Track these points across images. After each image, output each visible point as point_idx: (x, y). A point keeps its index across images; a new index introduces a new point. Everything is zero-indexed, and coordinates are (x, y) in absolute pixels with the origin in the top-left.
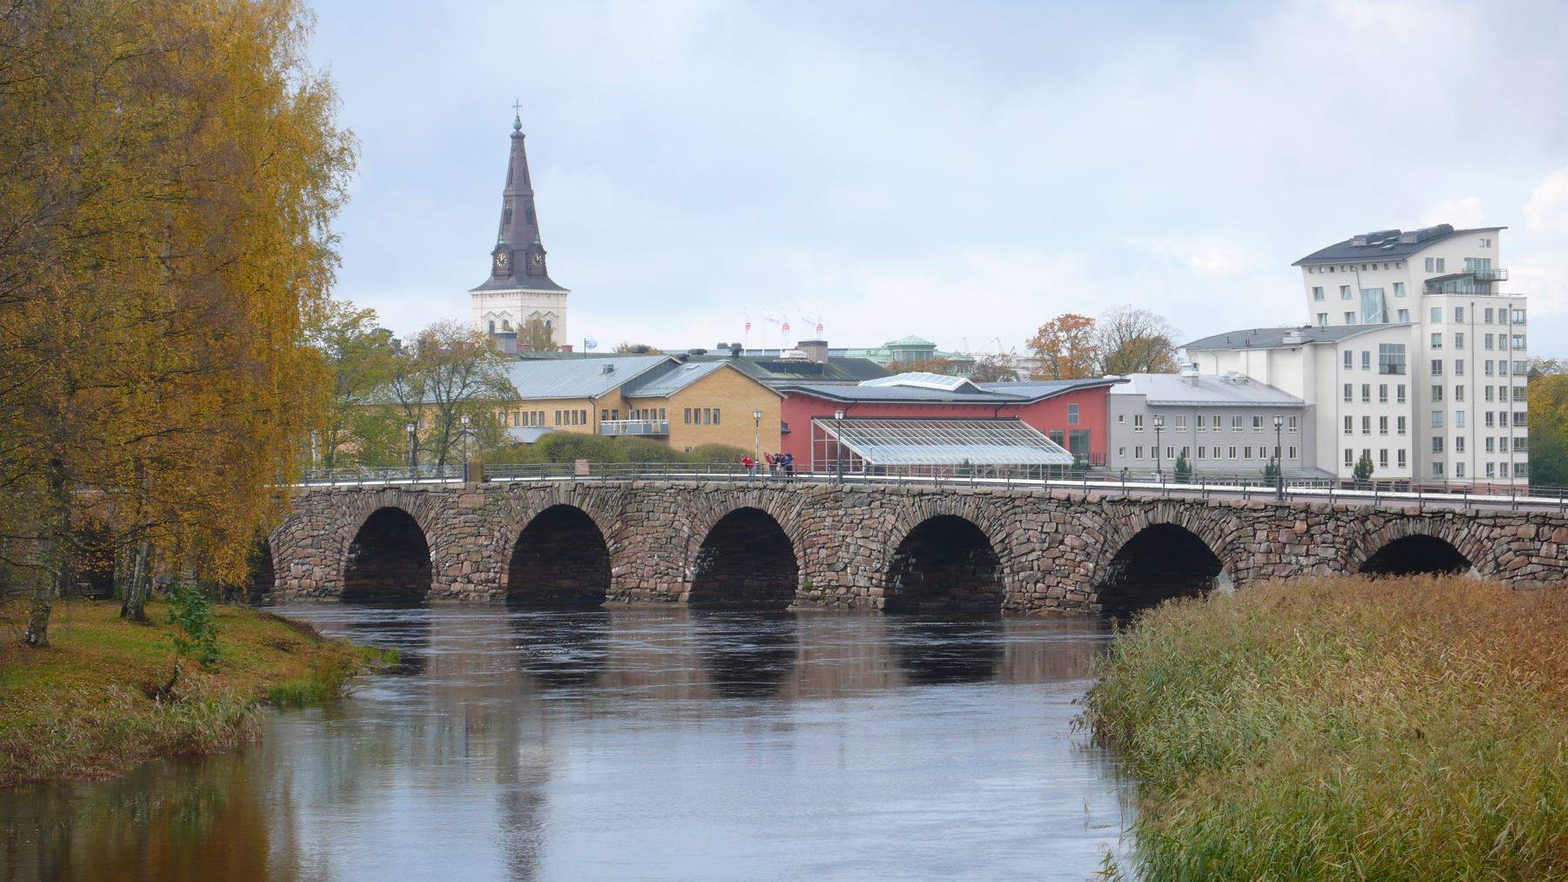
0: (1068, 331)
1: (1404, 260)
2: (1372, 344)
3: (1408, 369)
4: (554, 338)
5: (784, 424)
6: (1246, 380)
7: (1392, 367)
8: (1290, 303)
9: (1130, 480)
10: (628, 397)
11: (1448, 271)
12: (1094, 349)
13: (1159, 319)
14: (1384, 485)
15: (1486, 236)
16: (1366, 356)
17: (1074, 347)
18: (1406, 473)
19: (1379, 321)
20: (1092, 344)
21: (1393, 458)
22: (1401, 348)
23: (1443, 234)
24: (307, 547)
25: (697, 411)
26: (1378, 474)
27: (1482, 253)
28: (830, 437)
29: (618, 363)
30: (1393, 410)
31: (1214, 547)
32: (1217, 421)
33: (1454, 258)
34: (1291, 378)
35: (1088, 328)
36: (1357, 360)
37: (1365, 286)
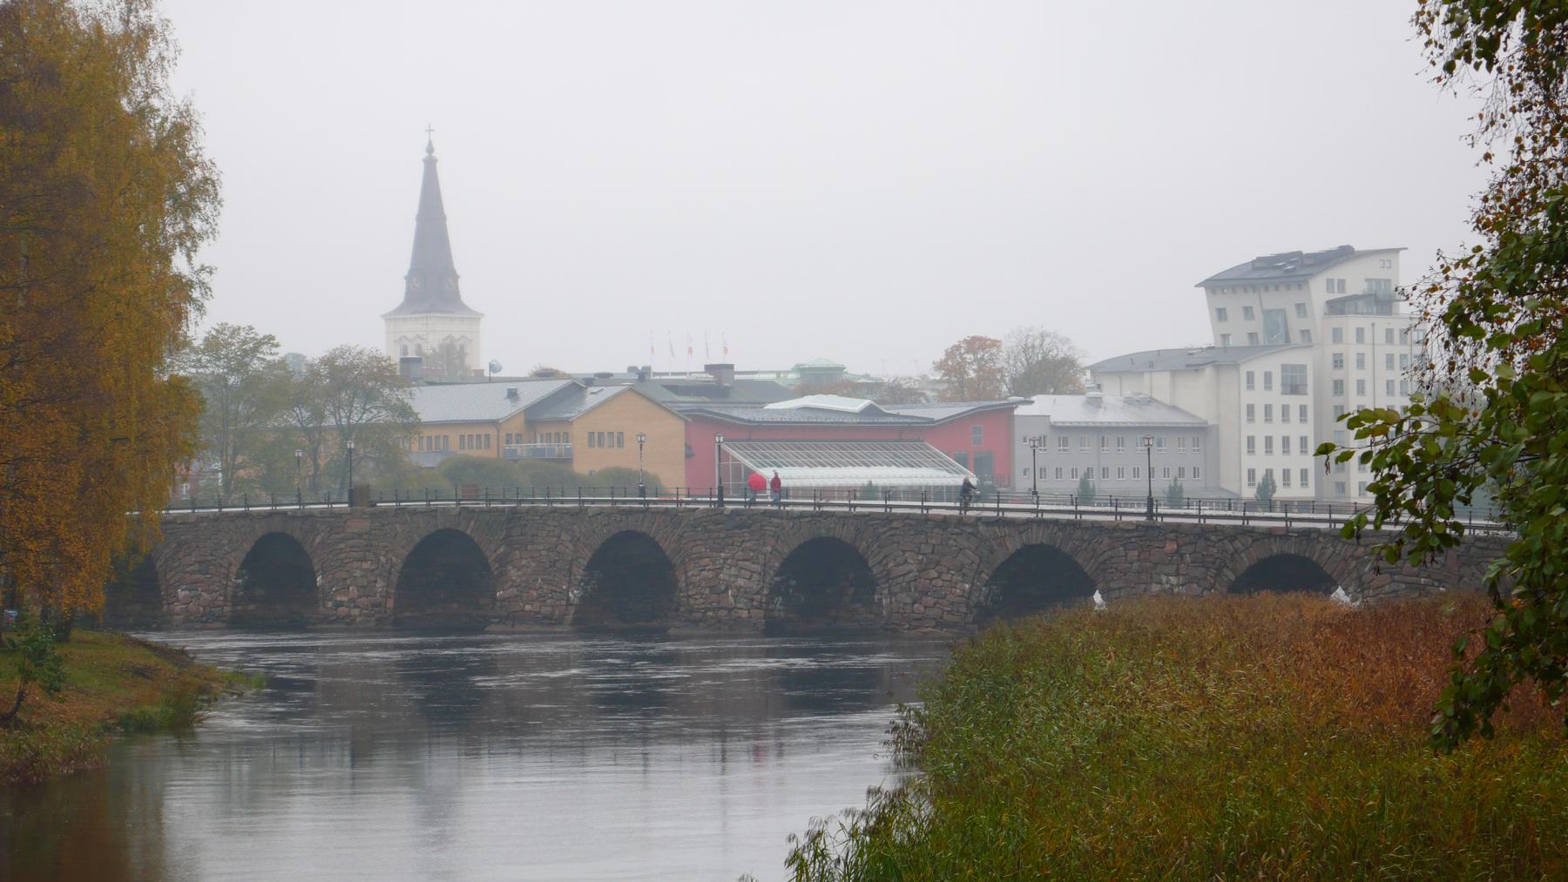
0: (975, 353)
1: (1306, 282)
2: (1273, 364)
3: (1310, 389)
4: (468, 361)
5: (688, 447)
6: (1151, 401)
7: (1294, 387)
8: (1194, 326)
9: (1006, 502)
10: (534, 417)
11: (1349, 292)
12: (1000, 370)
13: (1066, 341)
14: (1287, 505)
15: (1386, 257)
16: (1268, 377)
17: (980, 369)
18: (1309, 493)
19: (1281, 342)
20: (998, 366)
21: (1295, 477)
22: (1303, 368)
23: (1345, 254)
24: (193, 573)
25: (601, 434)
26: (1281, 493)
27: (1383, 274)
28: (735, 459)
29: (522, 389)
30: (1296, 430)
31: (1088, 569)
32: (1120, 443)
33: (1355, 279)
34: (1196, 399)
35: (994, 350)
36: (1259, 380)
37: (1267, 307)
